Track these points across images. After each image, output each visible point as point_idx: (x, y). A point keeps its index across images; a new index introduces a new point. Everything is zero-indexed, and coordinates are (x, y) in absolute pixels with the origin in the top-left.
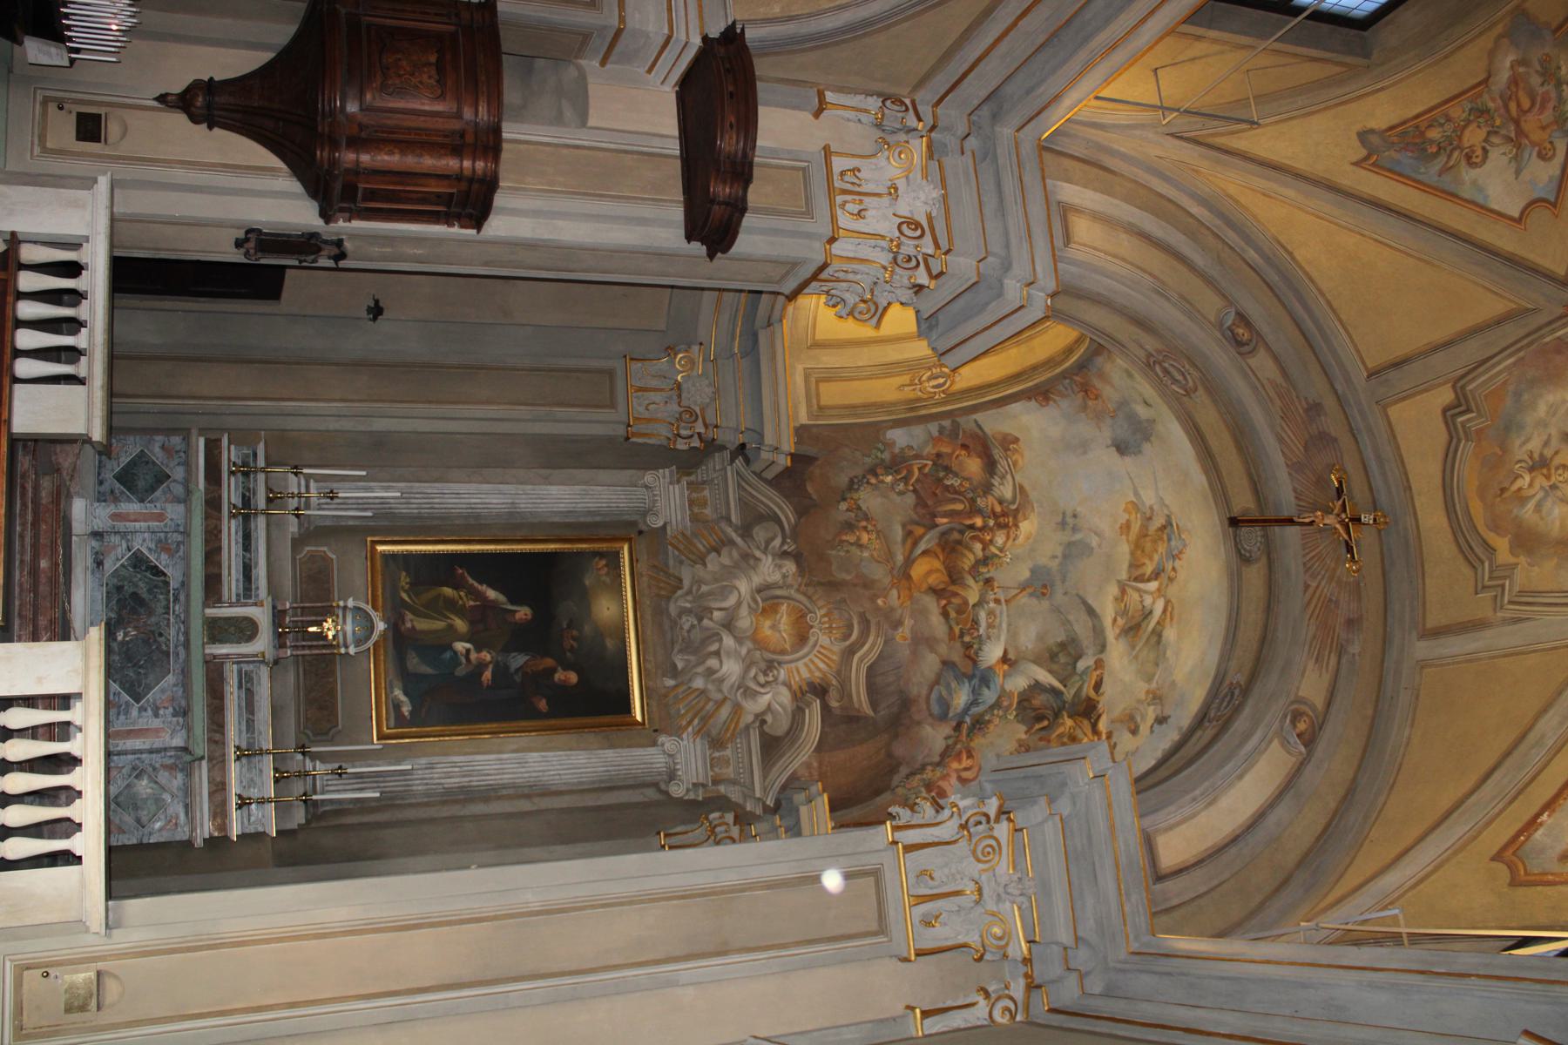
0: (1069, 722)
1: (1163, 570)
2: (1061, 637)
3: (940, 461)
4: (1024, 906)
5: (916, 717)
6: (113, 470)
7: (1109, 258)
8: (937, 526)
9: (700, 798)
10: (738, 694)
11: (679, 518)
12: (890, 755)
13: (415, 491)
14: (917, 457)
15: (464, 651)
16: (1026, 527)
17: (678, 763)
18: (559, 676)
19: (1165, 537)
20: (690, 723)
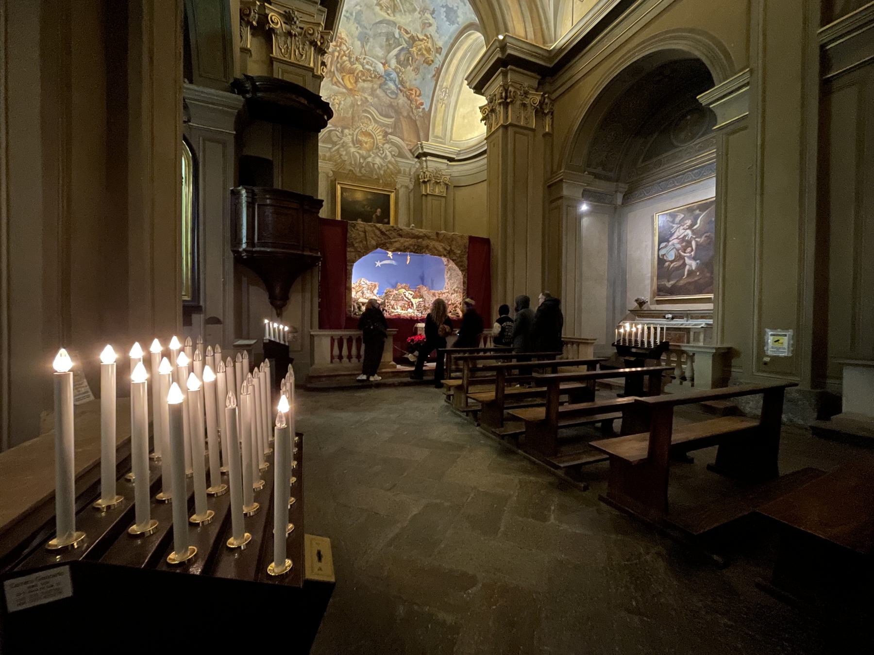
0: (414, 49)
20: (393, 178)
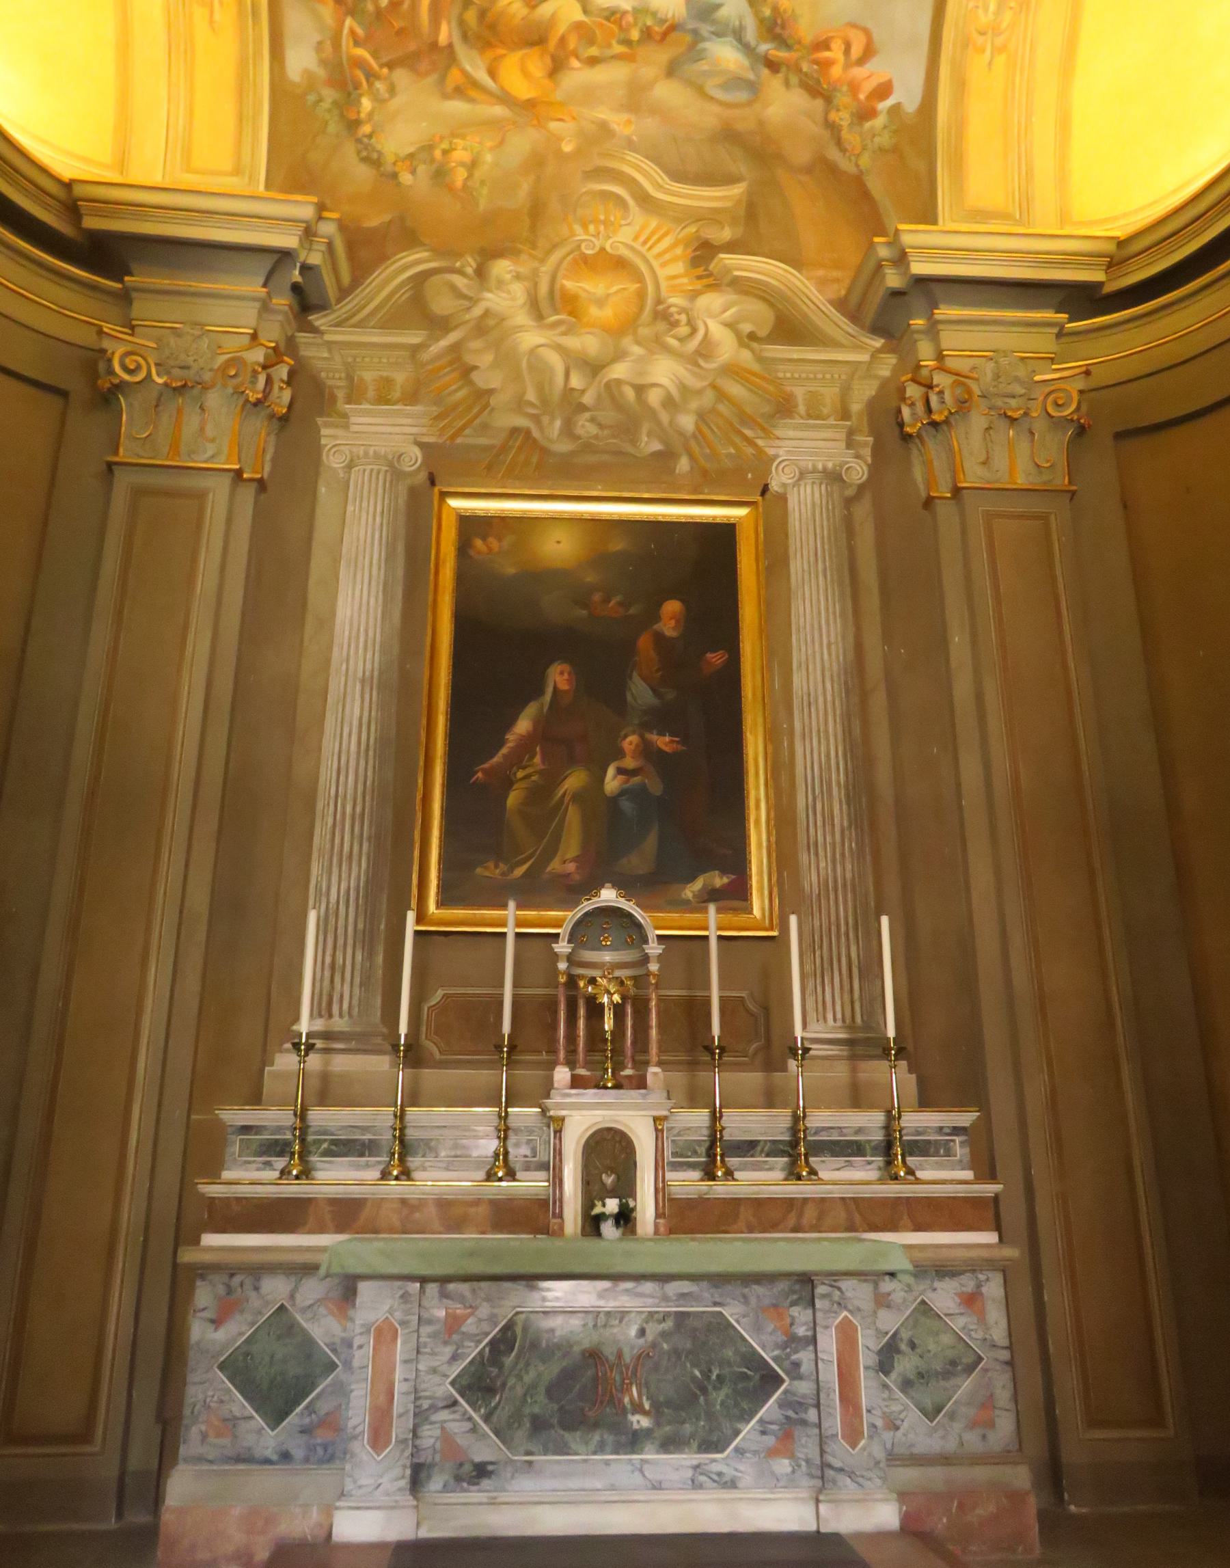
6: (260, 1431)
9: (871, 439)
11: (409, 421)
12: (809, 170)
13: (328, 846)
15: (620, 777)
17: (814, 466)
20: (750, 442)
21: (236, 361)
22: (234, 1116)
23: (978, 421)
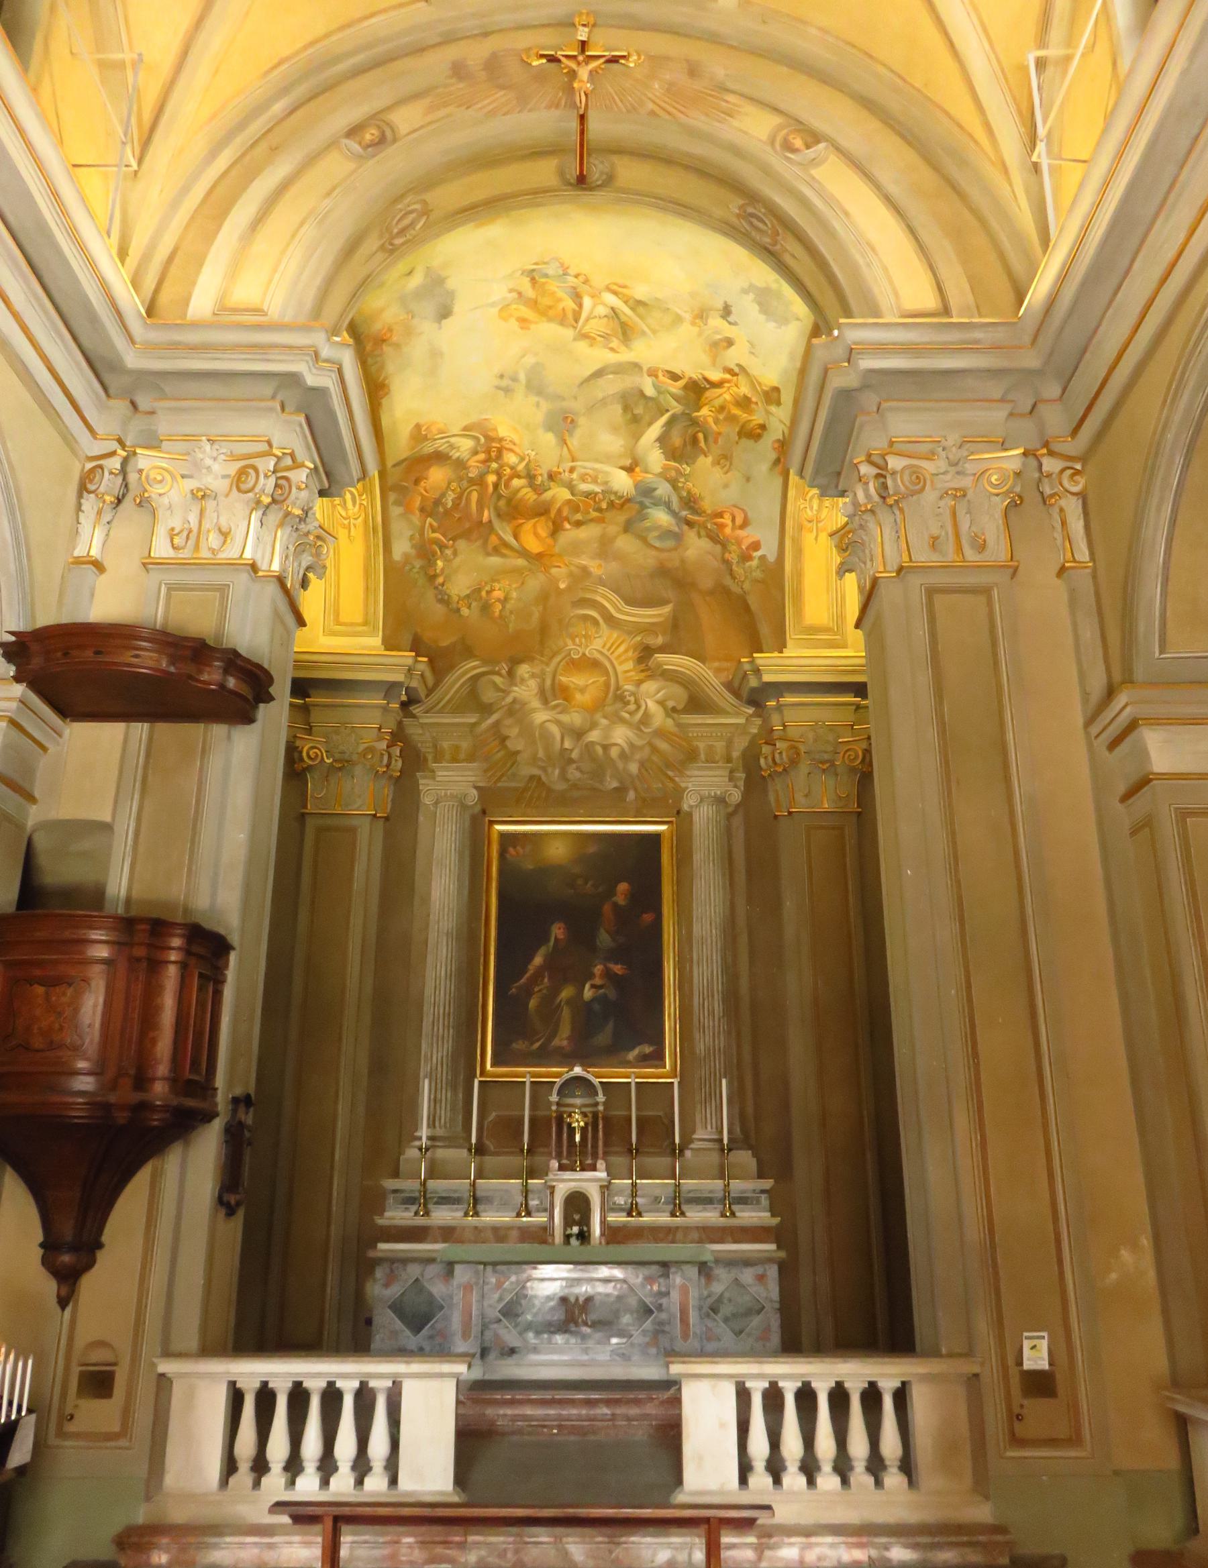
0: (705, 411)
1: (574, 288)
2: (618, 409)
3: (429, 509)
4: (971, 450)
5: (677, 563)
7: (282, 267)
8: (490, 521)
10: (646, 730)
11: (470, 773)
12: (711, 593)
14: (422, 533)
16: (503, 432)
18: (620, 899)
19: (543, 280)
21: (371, 749)
22: (390, 1184)
23: (804, 767)
